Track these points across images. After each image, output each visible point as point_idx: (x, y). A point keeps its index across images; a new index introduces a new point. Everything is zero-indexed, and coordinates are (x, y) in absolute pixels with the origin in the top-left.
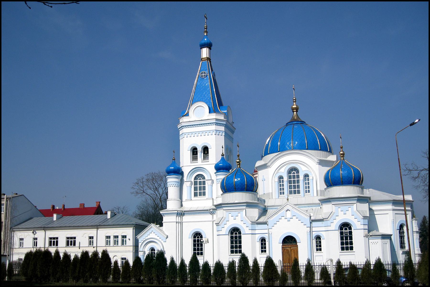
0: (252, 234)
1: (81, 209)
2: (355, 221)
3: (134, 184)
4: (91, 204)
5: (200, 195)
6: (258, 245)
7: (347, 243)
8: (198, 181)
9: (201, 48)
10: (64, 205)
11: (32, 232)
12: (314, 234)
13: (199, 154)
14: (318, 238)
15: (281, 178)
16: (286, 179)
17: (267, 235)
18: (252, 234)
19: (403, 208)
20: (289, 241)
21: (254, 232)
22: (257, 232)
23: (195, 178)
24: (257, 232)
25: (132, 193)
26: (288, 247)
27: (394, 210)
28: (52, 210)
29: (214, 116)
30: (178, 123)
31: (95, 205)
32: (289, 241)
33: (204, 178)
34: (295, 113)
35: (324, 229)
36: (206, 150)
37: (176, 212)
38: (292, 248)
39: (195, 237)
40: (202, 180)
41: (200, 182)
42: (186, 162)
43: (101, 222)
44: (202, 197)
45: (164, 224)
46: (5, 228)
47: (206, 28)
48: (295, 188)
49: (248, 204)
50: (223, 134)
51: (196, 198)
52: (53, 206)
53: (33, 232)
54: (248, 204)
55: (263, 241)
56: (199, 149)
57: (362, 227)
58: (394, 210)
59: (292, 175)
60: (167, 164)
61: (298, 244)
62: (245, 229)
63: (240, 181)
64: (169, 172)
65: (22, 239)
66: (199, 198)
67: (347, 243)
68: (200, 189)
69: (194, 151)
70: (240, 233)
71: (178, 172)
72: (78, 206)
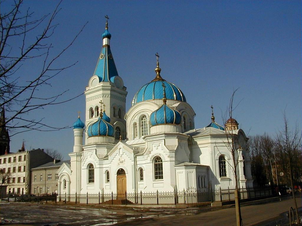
0: (99, 168)
2: (164, 154)
6: (104, 176)
7: (158, 173)
12: (138, 166)
14: (141, 170)
18: (99, 168)
19: (250, 189)
20: (19, 189)
21: (101, 166)
22: (104, 166)
24: (104, 166)
26: (120, 176)
27: (212, 143)
29: (102, 84)
32: (19, 189)
35: (144, 162)
37: (76, 154)
38: (123, 178)
45: (71, 162)
47: (158, 65)
50: (109, 96)
55: (108, 173)
56: (94, 109)
57: (168, 159)
58: (212, 143)
59: (143, 121)
61: (126, 175)
62: (96, 165)
64: (76, 127)
67: (158, 173)
70: (162, 161)
71: (82, 126)
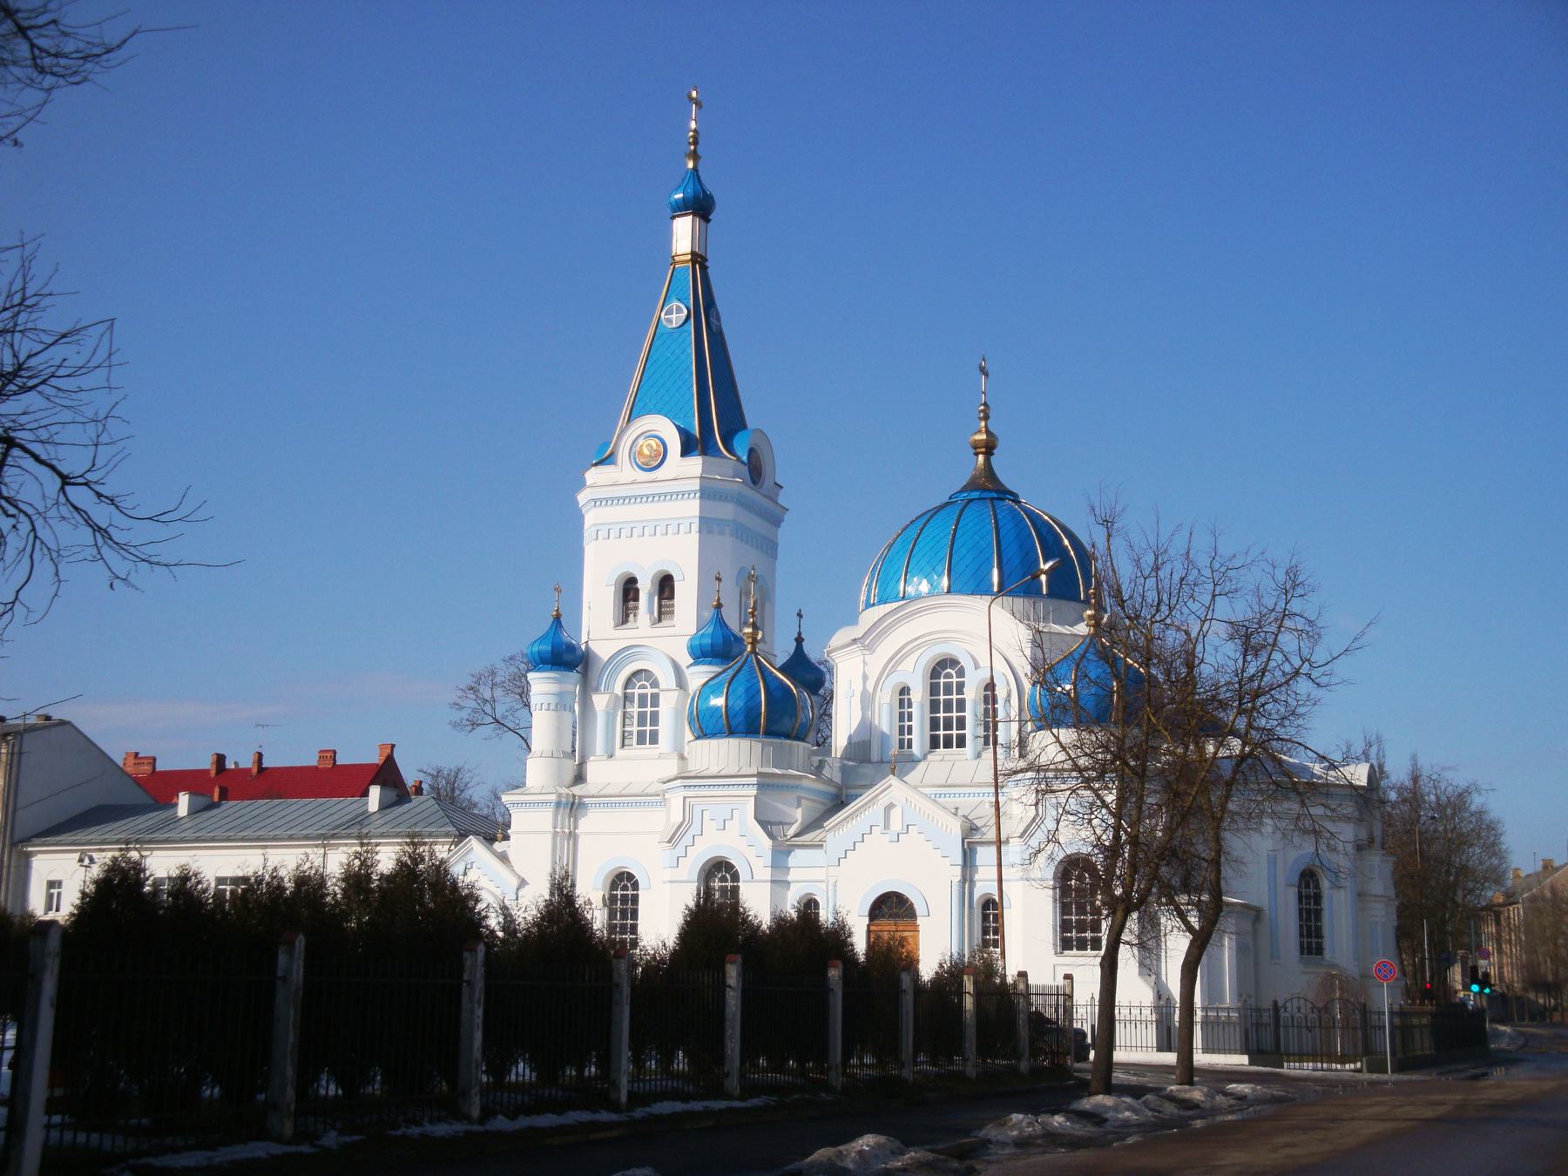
1: (327, 770)
3: (460, 693)
4: (360, 752)
5: (641, 739)
8: (637, 691)
9: (673, 218)
10: (260, 756)
11: (77, 856)
13: (643, 596)
15: (904, 691)
16: (919, 696)
17: (823, 886)
23: (628, 683)
25: (455, 725)
28: (255, 770)
30: (582, 484)
31: (375, 758)
33: (655, 684)
34: (981, 457)
36: (665, 585)
39: (614, 886)
40: (649, 691)
41: (643, 698)
42: (596, 628)
43: (337, 827)
44: (647, 750)
46: (783, 776)
47: (696, 143)
48: (948, 726)
49: (767, 781)
51: (626, 752)
52: (220, 759)
53: (81, 860)
54: (767, 781)
56: (645, 587)
60: (530, 634)
61: (919, 921)
63: (774, 701)
65: (52, 884)
66: (635, 750)
68: (642, 722)
69: (629, 590)
72: (311, 760)
